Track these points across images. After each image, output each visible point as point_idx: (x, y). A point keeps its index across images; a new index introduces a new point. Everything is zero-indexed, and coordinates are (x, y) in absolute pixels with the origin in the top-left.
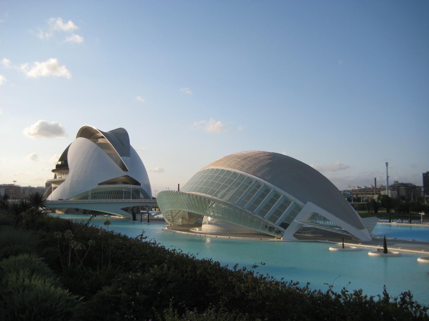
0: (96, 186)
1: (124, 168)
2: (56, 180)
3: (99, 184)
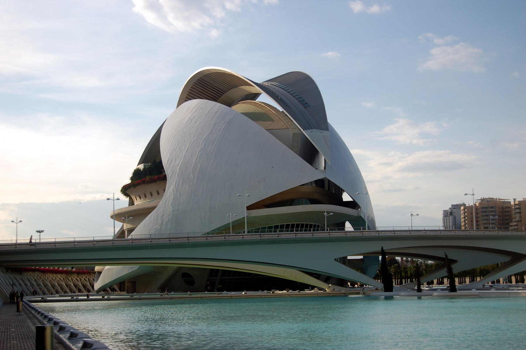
0: (244, 214)
2: (132, 208)
3: (249, 208)
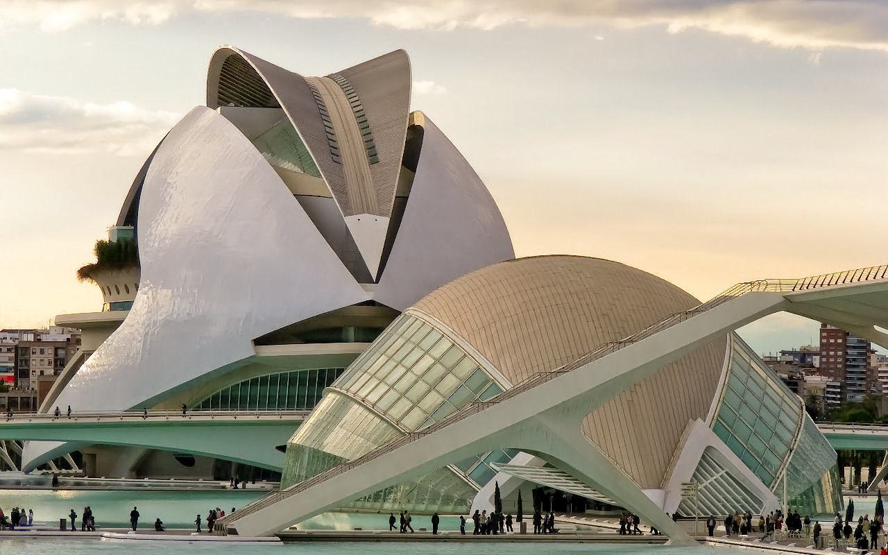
0: (246, 351)
1: (361, 274)
3: (259, 342)
